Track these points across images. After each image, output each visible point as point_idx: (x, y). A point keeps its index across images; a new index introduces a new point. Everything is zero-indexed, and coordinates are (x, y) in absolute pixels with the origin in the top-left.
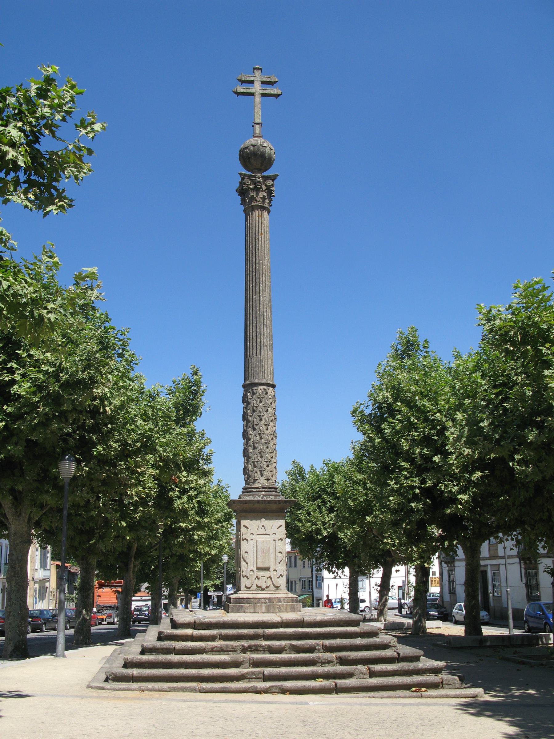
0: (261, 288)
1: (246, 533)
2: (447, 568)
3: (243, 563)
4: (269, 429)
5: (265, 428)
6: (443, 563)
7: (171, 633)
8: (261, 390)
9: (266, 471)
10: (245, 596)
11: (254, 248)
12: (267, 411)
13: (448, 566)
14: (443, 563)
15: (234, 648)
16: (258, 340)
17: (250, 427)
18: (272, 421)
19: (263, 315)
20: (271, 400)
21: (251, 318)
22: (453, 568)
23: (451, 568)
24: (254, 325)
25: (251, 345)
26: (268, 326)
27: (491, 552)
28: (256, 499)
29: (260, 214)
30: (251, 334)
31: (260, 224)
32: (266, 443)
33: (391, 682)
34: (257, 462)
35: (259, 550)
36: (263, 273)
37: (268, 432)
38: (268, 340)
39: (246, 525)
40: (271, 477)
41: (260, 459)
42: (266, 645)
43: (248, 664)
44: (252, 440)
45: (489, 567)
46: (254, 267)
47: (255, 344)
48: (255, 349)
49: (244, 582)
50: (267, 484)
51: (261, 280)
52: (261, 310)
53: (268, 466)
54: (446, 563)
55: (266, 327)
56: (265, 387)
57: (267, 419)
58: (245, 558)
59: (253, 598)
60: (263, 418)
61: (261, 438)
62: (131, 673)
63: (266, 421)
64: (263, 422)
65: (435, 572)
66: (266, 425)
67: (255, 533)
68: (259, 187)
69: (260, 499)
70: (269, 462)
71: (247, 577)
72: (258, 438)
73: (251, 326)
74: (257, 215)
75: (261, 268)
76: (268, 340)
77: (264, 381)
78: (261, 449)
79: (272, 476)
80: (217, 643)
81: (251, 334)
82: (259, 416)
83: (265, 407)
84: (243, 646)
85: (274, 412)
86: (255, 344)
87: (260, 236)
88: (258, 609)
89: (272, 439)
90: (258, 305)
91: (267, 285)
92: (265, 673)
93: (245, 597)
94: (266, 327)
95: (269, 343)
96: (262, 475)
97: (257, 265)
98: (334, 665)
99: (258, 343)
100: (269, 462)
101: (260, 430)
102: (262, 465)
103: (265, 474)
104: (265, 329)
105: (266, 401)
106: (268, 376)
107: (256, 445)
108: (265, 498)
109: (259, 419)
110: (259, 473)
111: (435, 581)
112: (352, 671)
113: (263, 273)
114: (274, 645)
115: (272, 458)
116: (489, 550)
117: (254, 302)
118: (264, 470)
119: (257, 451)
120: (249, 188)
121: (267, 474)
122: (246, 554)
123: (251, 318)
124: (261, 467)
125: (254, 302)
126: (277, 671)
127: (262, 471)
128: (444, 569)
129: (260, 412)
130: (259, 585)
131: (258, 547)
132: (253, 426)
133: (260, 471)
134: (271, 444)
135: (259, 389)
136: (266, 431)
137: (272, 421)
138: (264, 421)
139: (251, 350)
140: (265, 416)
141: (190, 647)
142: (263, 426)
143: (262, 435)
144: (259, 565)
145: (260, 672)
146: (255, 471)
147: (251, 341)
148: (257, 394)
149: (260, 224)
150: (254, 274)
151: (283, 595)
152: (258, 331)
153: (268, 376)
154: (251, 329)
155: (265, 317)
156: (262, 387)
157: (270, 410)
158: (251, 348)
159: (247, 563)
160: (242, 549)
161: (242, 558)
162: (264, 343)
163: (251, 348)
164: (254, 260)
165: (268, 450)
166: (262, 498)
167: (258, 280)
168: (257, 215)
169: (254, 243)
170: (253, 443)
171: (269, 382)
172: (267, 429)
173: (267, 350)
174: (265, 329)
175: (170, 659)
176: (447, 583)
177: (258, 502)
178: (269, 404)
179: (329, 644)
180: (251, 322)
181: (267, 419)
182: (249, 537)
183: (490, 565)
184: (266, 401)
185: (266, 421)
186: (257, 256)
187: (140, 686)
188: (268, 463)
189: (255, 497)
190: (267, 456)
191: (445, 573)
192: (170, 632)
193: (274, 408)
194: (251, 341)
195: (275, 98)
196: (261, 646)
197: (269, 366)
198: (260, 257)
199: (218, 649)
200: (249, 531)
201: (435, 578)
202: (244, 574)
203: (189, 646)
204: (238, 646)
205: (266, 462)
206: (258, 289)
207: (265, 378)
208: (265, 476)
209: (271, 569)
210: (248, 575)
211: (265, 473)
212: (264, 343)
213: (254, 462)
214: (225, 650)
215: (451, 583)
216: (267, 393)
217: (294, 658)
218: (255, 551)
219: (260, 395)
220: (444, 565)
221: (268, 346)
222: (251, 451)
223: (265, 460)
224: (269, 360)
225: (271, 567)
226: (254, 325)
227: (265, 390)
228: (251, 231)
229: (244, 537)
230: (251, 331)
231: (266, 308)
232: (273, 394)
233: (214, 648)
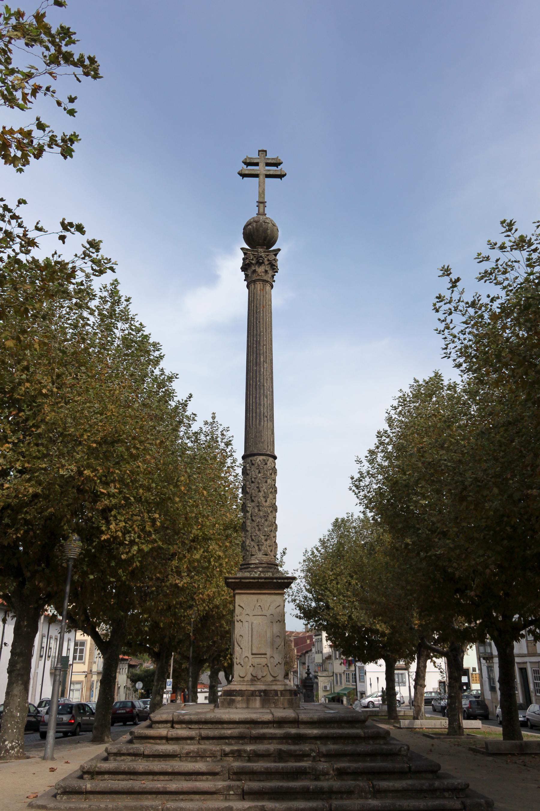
0: (262, 360)
1: (241, 614)
2: (486, 664)
3: (237, 648)
4: (268, 501)
5: (263, 500)
6: (482, 659)
7: (142, 733)
8: (260, 460)
9: (265, 546)
10: (238, 688)
11: (255, 320)
12: (266, 482)
13: (486, 662)
14: (482, 659)
15: (214, 754)
16: (258, 411)
17: (248, 500)
18: (271, 492)
19: (264, 386)
20: (271, 471)
21: (251, 390)
22: (492, 665)
23: (489, 665)
24: (254, 395)
25: (251, 416)
26: (268, 397)
27: (529, 648)
28: (252, 576)
29: (262, 288)
30: (251, 404)
31: (262, 297)
32: (265, 516)
33: (400, 805)
34: (255, 536)
35: (255, 633)
36: (264, 345)
37: (267, 504)
38: (269, 411)
39: (241, 605)
40: (269, 552)
41: (258, 533)
42: (250, 750)
43: (227, 775)
44: (250, 513)
45: (528, 664)
46: (255, 339)
47: (254, 415)
48: (254, 419)
49: (237, 670)
50: (265, 559)
51: (262, 351)
52: (262, 381)
53: (266, 540)
54: (484, 659)
55: (267, 398)
56: (264, 457)
57: (266, 490)
58: (239, 643)
59: (246, 690)
60: (261, 489)
61: (259, 510)
62: (84, 787)
63: (265, 492)
64: (261, 494)
65: (475, 668)
66: (264, 497)
67: (251, 614)
68: (261, 261)
69: (257, 575)
70: (268, 536)
71: (241, 665)
72: (256, 510)
73: (251, 397)
74: (259, 289)
75: (262, 340)
76: (269, 411)
77: (264, 452)
78: (259, 522)
79: (271, 551)
80: (192, 747)
81: (251, 404)
82: (258, 487)
83: (263, 478)
84: (224, 751)
85: (273, 483)
86: (254, 415)
87: (262, 309)
88: (252, 705)
89: (272, 512)
90: (258, 376)
91: (268, 357)
92: (245, 788)
93: (238, 689)
94: (267, 398)
95: (269, 414)
96: (260, 550)
97: (258, 337)
98: (331, 779)
99: (258, 413)
100: (268, 536)
101: (258, 502)
102: (260, 539)
103: (263, 549)
104: (266, 399)
105: (266, 472)
106: (268, 446)
107: (254, 518)
108: (262, 575)
109: (257, 490)
110: (257, 548)
111: (476, 677)
112: (352, 788)
113: (264, 345)
114: (260, 750)
115: (271, 531)
116: (527, 646)
117: (254, 373)
118: (262, 545)
119: (255, 524)
120: (252, 263)
121: (266, 549)
122: (240, 638)
123: (251, 390)
124: (258, 542)
125: (254, 373)
126: (259, 786)
127: (260, 546)
128: (482, 665)
129: (258, 483)
130: (254, 675)
131: (254, 630)
132: (251, 497)
133: (258, 545)
134: (270, 517)
135: (258, 460)
136: (264, 504)
137: (271, 492)
138: (262, 492)
139: (251, 421)
140: (264, 488)
141: (162, 752)
142: (262, 498)
143: (261, 508)
144: (254, 652)
145: (238, 787)
146: (252, 546)
147: (251, 412)
148: (256, 465)
149: (262, 297)
150: (255, 346)
151: (280, 687)
152: (258, 401)
153: (268, 446)
154: (251, 400)
155: (265, 388)
156: (261, 458)
157: (269, 481)
158: (251, 418)
159: (241, 648)
160: (236, 632)
161: (236, 643)
162: (264, 413)
163: (251, 418)
164: (255, 332)
165: (266, 523)
166: (260, 574)
167: (258, 351)
168: (259, 289)
169: (255, 315)
170: (251, 516)
171: (268, 453)
172: (266, 501)
173: (267, 420)
174: (266, 399)
175: (134, 768)
176: (487, 680)
177: (254, 578)
178: (269, 475)
179: (326, 751)
180: (251, 393)
181: (266, 490)
182: (243, 618)
183: (530, 662)
184: (266, 472)
185: (265, 492)
186: (258, 328)
187: (90, 804)
188: (266, 537)
189: (251, 574)
190: (266, 529)
191: (485, 669)
192: (142, 731)
193: (273, 480)
194: (251, 412)
195: (279, 179)
196: (245, 751)
197: (269, 436)
198: (262, 329)
199: (195, 754)
200: (244, 612)
201: (476, 674)
202: (238, 661)
203: (160, 750)
204: (218, 751)
205: (264, 536)
206: (258, 361)
207: (264, 449)
208: (262, 551)
209: (268, 656)
210: (242, 663)
211: (263, 548)
212: (264, 413)
213: (251, 536)
214: (202, 755)
215: (491, 679)
216: (266, 464)
217: (283, 768)
218: (250, 635)
219: (258, 465)
220: (483, 661)
221: (268, 417)
222: (249, 524)
223: (264, 534)
224: (269, 431)
225: (268, 653)
226: (254, 395)
227: (264, 460)
228: (252, 305)
229: (238, 618)
230: (251, 402)
231: (267, 379)
232: (273, 466)
233: (190, 753)
